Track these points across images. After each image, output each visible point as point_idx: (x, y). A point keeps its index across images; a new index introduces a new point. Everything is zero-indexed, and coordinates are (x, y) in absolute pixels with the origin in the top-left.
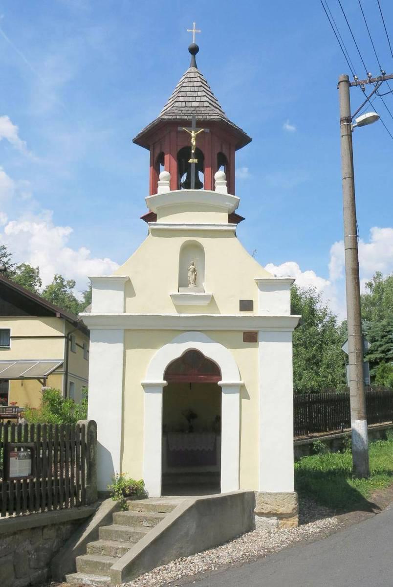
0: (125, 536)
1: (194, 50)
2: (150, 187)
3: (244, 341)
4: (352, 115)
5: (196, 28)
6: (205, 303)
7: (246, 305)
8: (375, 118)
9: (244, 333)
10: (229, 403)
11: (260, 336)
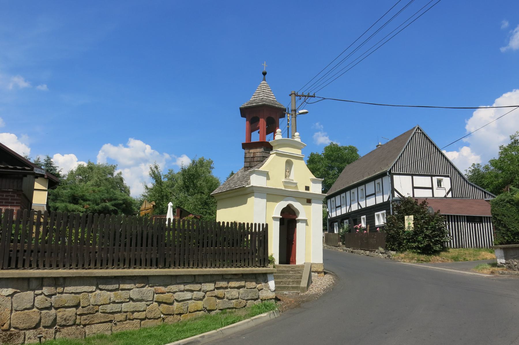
0: (288, 277)
1: (264, 74)
2: (246, 131)
3: (307, 202)
4: (296, 109)
5: (266, 64)
6: (294, 186)
7: (307, 188)
8: (307, 113)
9: (307, 199)
10: (299, 226)
11: (312, 201)
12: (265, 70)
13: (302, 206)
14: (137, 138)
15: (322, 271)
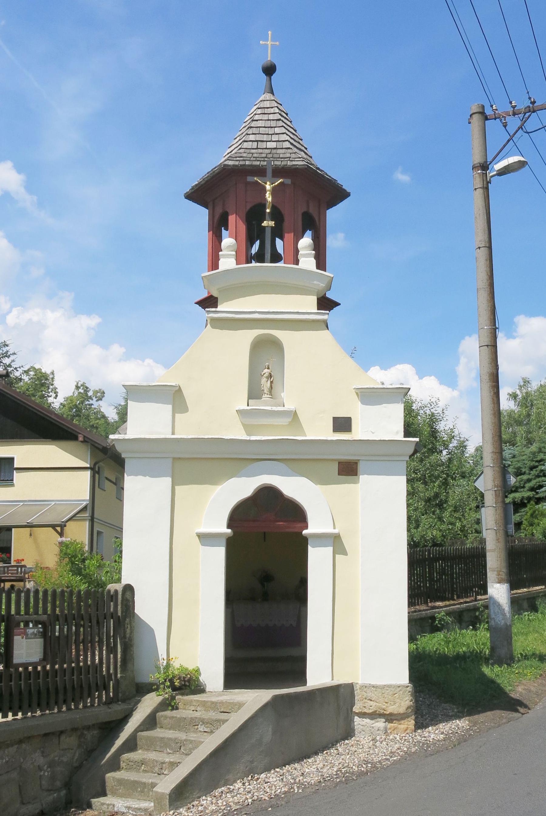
0: (173, 745)
3: (339, 474)
4: (489, 160)
6: (285, 421)
8: (521, 164)
9: (339, 463)
12: (269, 58)
13: (319, 487)
14: (532, 313)
15: (402, 712)
